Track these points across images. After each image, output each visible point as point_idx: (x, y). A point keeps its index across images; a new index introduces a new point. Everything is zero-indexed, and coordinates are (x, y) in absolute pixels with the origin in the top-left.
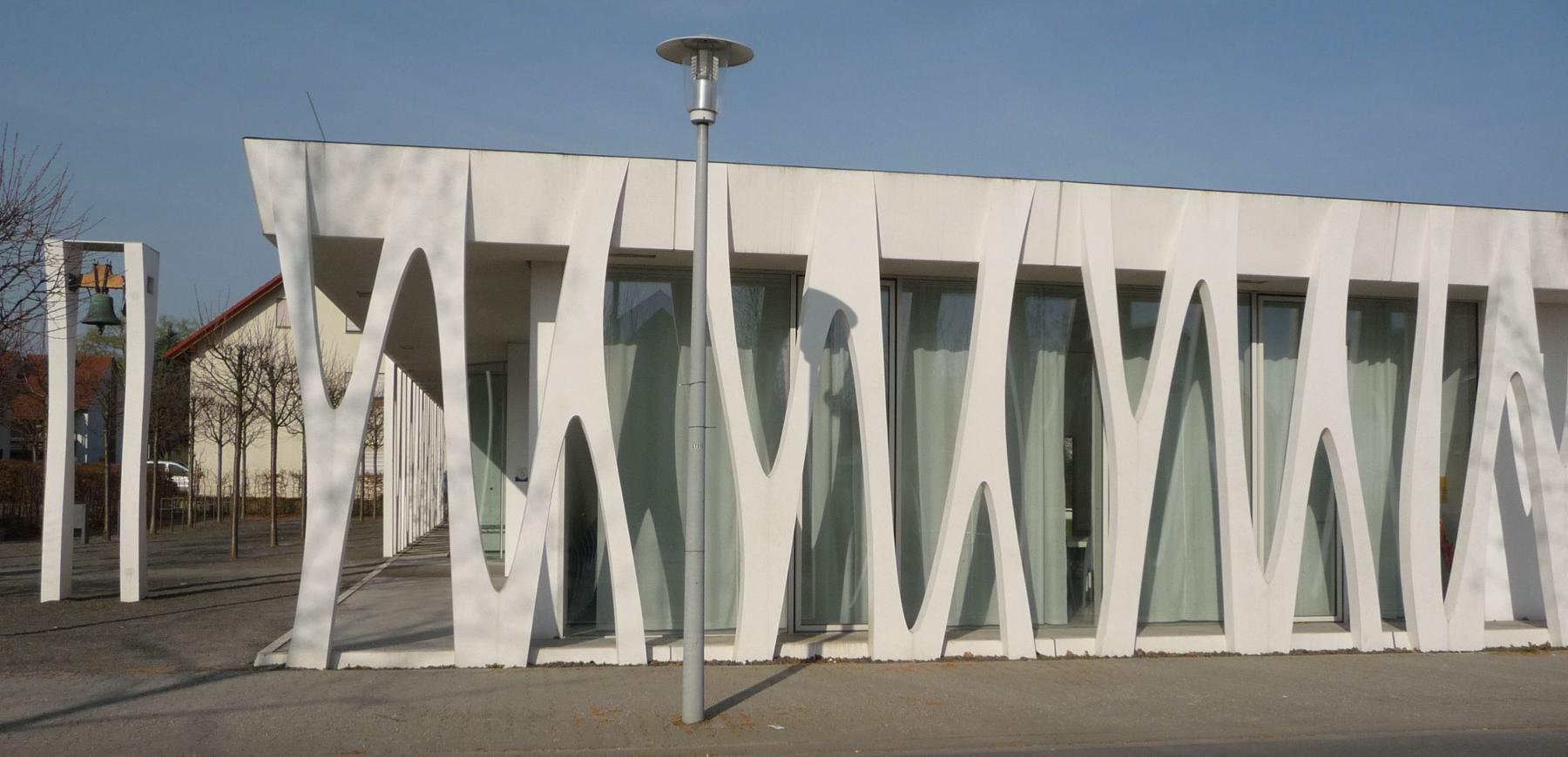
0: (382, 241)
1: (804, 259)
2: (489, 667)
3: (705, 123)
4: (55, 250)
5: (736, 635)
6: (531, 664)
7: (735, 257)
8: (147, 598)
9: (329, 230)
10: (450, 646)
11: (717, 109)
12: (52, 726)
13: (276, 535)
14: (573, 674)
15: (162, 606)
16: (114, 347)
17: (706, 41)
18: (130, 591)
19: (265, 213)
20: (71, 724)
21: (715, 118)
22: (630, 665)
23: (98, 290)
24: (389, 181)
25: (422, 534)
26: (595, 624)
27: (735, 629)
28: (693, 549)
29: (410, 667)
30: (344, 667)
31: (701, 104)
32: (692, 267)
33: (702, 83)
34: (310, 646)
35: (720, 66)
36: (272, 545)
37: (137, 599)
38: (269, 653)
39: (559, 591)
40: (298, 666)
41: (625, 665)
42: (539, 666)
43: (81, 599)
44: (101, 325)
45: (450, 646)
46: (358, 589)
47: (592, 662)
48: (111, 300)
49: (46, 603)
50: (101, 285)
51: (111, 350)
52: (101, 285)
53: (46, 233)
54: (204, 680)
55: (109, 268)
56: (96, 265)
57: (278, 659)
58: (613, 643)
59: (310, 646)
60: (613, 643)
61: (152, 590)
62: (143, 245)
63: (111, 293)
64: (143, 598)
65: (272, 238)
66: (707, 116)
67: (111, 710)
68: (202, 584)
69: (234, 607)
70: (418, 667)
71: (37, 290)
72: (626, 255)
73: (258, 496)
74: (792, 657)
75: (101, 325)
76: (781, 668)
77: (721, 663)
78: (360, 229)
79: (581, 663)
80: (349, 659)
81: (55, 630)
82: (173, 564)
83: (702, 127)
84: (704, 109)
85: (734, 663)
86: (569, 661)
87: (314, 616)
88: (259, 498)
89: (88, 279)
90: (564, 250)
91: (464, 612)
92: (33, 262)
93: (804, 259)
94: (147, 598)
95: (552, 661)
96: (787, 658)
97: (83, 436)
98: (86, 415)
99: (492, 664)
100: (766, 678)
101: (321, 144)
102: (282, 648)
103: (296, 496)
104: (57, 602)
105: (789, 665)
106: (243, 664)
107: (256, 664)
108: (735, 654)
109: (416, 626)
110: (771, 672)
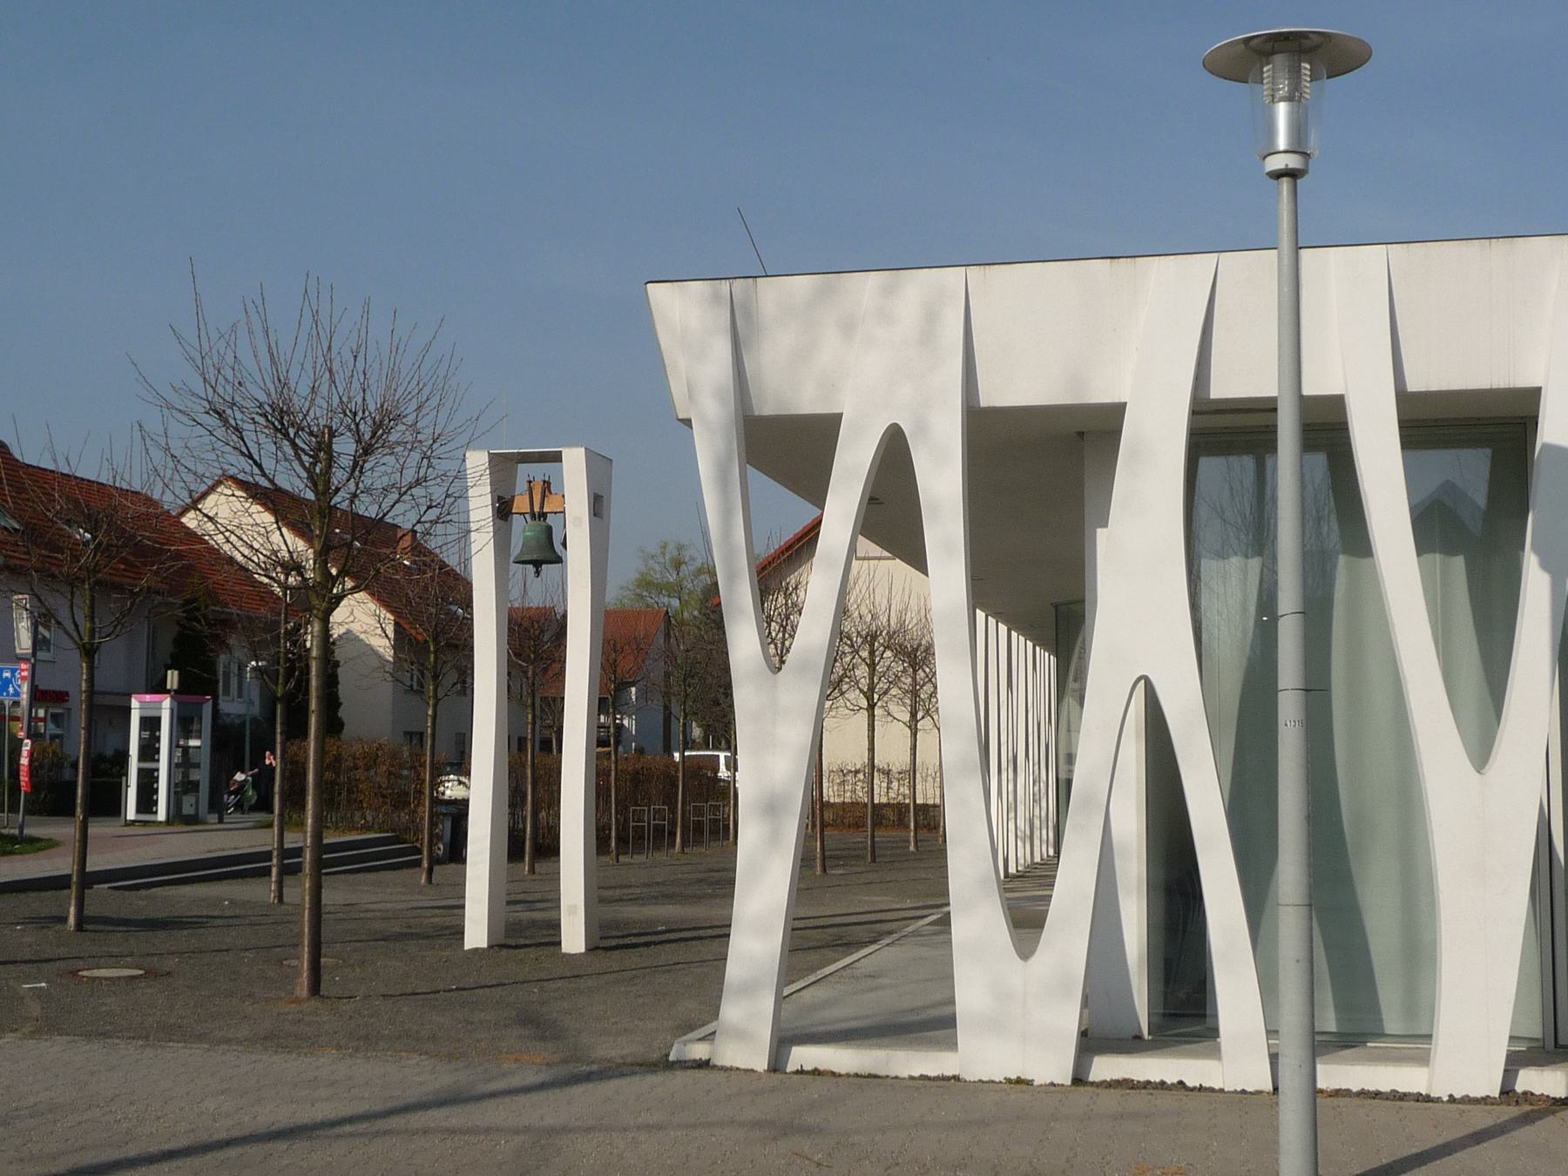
0: (841, 415)
1: (1533, 395)
2: (1009, 1081)
3: (1292, 174)
4: (477, 461)
5: (1432, 1046)
6: (1079, 1080)
7: (1405, 399)
8: (597, 948)
9: (766, 407)
10: (952, 1045)
11: (1313, 146)
12: (351, 1135)
13: (824, 859)
14: (1138, 1100)
15: (614, 960)
16: (669, 596)
17: (1286, 37)
18: (573, 938)
19: (677, 389)
20: (377, 1134)
21: (1307, 164)
22: (1243, 1092)
23: (533, 516)
24: (848, 328)
25: (1037, 859)
26: (1205, 1016)
27: (1430, 1036)
28: (1290, 901)
29: (893, 1074)
30: (794, 1069)
31: (1282, 142)
32: (1275, 426)
33: (1282, 109)
34: (741, 1035)
35: (1313, 78)
36: (818, 873)
37: (583, 950)
38: (691, 1041)
39: (1139, 957)
40: (728, 1064)
41: (1235, 1092)
42: (1092, 1084)
43: (517, 947)
44: (537, 564)
45: (952, 1045)
46: (888, 945)
47: (1181, 1083)
48: (549, 529)
49: (470, 950)
50: (537, 509)
51: (666, 600)
52: (537, 509)
53: (434, 442)
54: (588, 1077)
55: (547, 485)
56: (530, 482)
57: (699, 1051)
58: (1216, 1053)
59: (741, 1035)
60: (1216, 1053)
61: (603, 937)
62: (586, 449)
63: (550, 520)
64: (592, 948)
65: (687, 422)
66: (1293, 161)
67: (437, 1117)
68: (681, 930)
69: (702, 966)
70: (905, 1074)
71: (422, 520)
72: (1218, 412)
73: (832, 801)
74: (1537, 1092)
75: (537, 564)
76: (1513, 1111)
77: (1403, 1097)
78: (808, 403)
79: (1163, 1083)
80: (804, 1056)
81: (452, 990)
82: (669, 898)
83: (1285, 183)
84: (1285, 152)
85: (1428, 1099)
86: (1142, 1079)
87: (748, 989)
88: (835, 803)
89: (521, 504)
90: (1118, 410)
91: (970, 995)
92: (418, 483)
93: (1533, 395)
94: (597, 948)
95: (1115, 1077)
96: (1527, 1095)
97: (630, 716)
98: (633, 689)
99: (1014, 1077)
100: (1471, 1130)
101: (751, 280)
102: (710, 1037)
103: (450, 818)
104: (483, 949)
105: (1527, 1108)
106: (655, 1056)
107: (671, 1058)
108: (1430, 1084)
109: (934, 1006)
110: (1482, 1119)
